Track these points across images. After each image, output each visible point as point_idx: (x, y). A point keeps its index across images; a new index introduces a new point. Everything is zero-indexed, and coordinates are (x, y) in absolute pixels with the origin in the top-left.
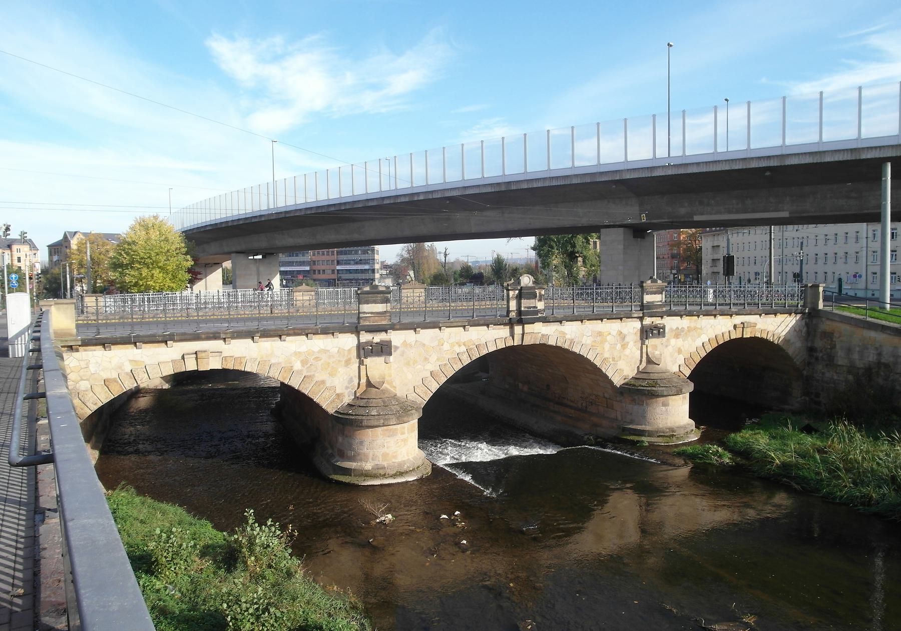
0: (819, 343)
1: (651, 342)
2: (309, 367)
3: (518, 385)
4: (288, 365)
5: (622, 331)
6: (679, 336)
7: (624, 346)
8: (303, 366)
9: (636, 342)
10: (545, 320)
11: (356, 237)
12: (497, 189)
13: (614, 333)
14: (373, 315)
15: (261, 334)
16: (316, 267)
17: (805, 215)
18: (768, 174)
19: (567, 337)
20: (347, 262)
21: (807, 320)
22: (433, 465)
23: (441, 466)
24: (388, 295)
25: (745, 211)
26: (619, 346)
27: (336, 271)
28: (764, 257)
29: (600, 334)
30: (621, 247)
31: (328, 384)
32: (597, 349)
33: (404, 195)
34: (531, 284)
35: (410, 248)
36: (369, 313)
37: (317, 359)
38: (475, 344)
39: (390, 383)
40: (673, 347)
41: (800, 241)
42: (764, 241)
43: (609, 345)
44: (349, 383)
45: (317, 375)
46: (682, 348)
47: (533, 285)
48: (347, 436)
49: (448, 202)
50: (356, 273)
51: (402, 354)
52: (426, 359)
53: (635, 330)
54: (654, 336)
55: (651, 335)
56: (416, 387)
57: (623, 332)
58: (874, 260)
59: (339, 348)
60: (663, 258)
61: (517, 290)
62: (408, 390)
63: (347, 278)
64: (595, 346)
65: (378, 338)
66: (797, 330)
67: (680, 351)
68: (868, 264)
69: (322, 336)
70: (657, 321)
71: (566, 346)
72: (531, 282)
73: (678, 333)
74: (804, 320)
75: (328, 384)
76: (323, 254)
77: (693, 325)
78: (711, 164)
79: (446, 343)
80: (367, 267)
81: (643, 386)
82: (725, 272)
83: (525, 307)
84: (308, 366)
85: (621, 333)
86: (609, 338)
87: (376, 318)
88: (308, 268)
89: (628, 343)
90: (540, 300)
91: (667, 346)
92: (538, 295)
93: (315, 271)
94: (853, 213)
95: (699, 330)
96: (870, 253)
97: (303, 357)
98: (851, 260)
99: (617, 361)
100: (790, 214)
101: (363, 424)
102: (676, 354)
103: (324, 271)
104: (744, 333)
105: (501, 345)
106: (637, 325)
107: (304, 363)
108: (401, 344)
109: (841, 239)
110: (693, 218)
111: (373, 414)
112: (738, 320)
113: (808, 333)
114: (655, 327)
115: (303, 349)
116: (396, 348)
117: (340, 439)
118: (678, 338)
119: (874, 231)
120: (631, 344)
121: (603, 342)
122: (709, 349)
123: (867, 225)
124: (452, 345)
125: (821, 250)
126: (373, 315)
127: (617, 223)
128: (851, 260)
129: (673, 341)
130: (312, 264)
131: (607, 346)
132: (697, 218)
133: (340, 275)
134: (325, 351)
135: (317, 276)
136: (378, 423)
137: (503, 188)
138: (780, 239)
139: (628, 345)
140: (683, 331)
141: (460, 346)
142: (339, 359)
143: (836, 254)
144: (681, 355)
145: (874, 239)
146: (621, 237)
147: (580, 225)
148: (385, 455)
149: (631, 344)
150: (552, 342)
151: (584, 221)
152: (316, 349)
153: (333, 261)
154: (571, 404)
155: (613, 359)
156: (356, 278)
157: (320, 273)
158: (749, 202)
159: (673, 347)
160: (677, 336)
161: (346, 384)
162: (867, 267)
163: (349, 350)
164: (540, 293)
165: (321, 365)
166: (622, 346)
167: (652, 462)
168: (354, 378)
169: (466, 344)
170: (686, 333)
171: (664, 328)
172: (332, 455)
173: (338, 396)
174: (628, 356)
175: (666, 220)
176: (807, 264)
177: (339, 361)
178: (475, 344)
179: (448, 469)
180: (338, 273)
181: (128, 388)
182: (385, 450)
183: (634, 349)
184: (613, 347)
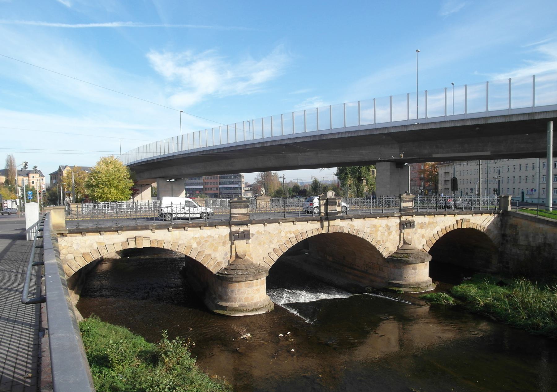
0: (508, 232)
1: (406, 231)
4: (189, 245)
5: (388, 224)
7: (390, 234)
8: (198, 245)
11: (230, 168)
12: (314, 139)
15: (173, 227)
16: (207, 186)
17: (500, 153)
18: (477, 128)
20: (225, 183)
26: (386, 234)
29: (375, 226)
30: (389, 173)
31: (213, 256)
34: (333, 196)
35: (263, 175)
36: (236, 214)
37: (206, 241)
38: (300, 233)
42: (501, 167)
47: (334, 197)
49: (284, 147)
51: (257, 238)
52: (271, 242)
54: (407, 227)
55: (406, 227)
59: (219, 235)
60: (415, 180)
62: (260, 260)
65: (242, 229)
67: (423, 236)
68: (540, 183)
71: (354, 234)
72: (334, 195)
73: (422, 226)
75: (213, 256)
77: (431, 221)
80: (237, 186)
81: (401, 258)
84: (201, 245)
88: (202, 187)
89: (392, 231)
91: (415, 233)
92: (337, 203)
93: (206, 188)
97: (198, 240)
98: (530, 181)
99: (385, 243)
100: (491, 153)
103: (211, 188)
104: (463, 225)
105: (316, 233)
106: (397, 220)
107: (198, 243)
109: (523, 167)
116: (253, 235)
117: (220, 289)
120: (394, 232)
121: (376, 231)
122: (441, 235)
124: (286, 233)
127: (386, 159)
128: (530, 181)
129: (419, 231)
130: (204, 184)
131: (379, 233)
132: (434, 156)
133: (221, 191)
134: (211, 237)
135: (207, 192)
136: (242, 279)
137: (317, 139)
141: (291, 233)
143: (514, 177)
144: (424, 239)
145: (544, 168)
146: (389, 168)
147: (364, 161)
149: (394, 232)
151: (366, 158)
155: (383, 241)
157: (209, 190)
160: (422, 227)
163: (225, 236)
164: (339, 202)
168: (228, 252)
169: (295, 232)
171: (413, 222)
173: (219, 263)
174: (392, 239)
175: (416, 157)
176: (502, 183)
180: (220, 190)
184: (383, 234)
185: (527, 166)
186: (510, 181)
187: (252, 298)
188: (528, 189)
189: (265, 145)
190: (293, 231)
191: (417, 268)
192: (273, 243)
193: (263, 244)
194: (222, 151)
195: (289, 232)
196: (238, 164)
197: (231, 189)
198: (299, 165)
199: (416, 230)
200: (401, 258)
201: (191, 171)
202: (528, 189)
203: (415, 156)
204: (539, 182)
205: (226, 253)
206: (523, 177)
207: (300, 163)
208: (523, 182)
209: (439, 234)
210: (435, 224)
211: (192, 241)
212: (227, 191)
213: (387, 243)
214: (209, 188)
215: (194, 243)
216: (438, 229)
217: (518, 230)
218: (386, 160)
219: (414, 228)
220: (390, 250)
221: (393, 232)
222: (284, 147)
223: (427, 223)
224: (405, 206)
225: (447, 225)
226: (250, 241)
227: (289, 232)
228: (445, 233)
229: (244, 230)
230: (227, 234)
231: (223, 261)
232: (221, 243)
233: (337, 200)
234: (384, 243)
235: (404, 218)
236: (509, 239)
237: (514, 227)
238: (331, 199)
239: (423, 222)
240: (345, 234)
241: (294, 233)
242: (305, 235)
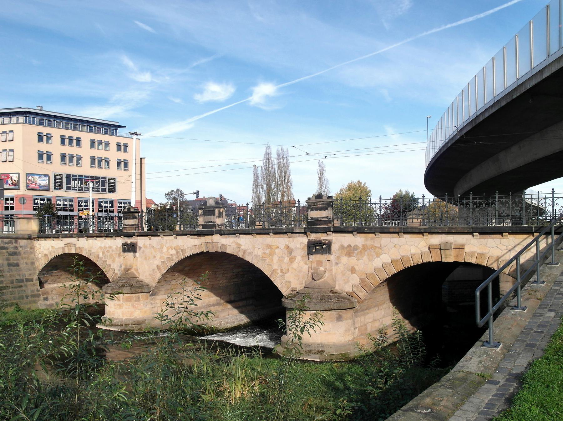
1: (316, 258)
5: (289, 245)
6: (352, 255)
7: (292, 260)
9: (303, 257)
10: (221, 233)
13: (282, 247)
26: (286, 259)
29: (269, 247)
32: (265, 260)
36: (126, 225)
39: (136, 270)
40: (344, 265)
43: (277, 258)
44: (120, 268)
53: (302, 246)
54: (317, 252)
56: (354, 286)
64: (265, 257)
70: (323, 237)
73: (350, 251)
77: (369, 243)
79: (164, 247)
83: (205, 222)
85: (289, 247)
86: (277, 251)
87: (129, 228)
95: (377, 249)
99: (285, 273)
102: (350, 273)
106: (303, 240)
107: (103, 253)
112: (436, 240)
115: (103, 245)
116: (140, 248)
120: (299, 258)
121: (272, 254)
124: (168, 249)
131: (276, 258)
134: (110, 247)
139: (295, 259)
140: (357, 249)
144: (354, 275)
149: (299, 258)
150: (229, 251)
159: (344, 265)
166: (289, 259)
169: (176, 248)
170: (361, 252)
183: (302, 263)
184: (281, 260)
216: (386, 258)
220: (293, 286)
223: (360, 246)
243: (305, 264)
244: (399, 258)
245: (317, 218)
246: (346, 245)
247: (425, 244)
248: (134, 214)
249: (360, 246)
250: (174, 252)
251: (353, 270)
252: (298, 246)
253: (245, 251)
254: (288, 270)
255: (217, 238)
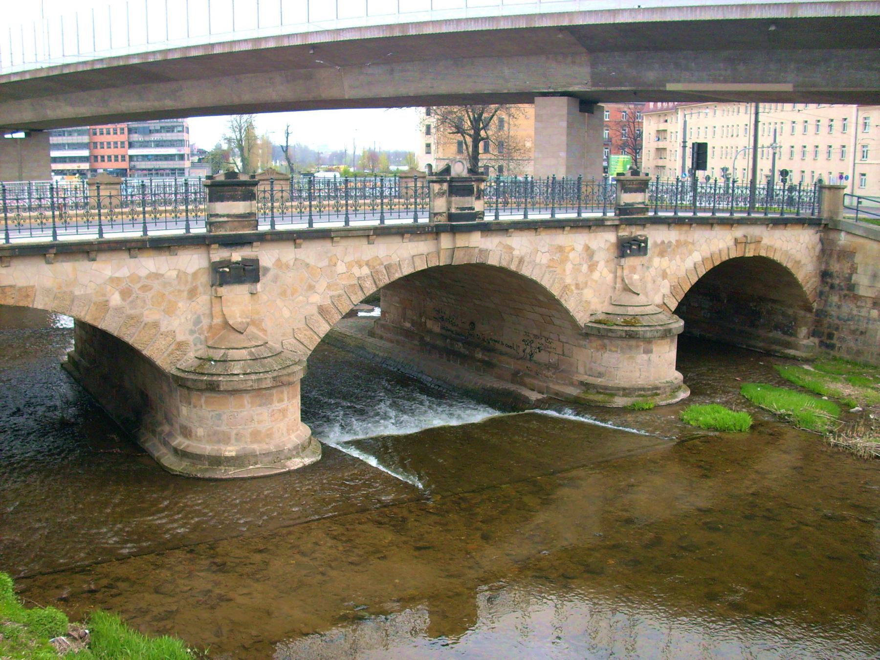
0: (835, 267)
1: (629, 262)
2: (132, 302)
3: (425, 322)
4: (101, 298)
5: (590, 245)
7: (592, 267)
8: (123, 299)
11: (169, 104)
12: (387, 34)
14: (230, 219)
15: (57, 250)
17: (812, 89)
18: (772, 28)
19: (514, 253)
20: (145, 144)
21: (822, 234)
22: (322, 444)
23: (333, 446)
24: (253, 188)
25: (735, 81)
26: (585, 268)
27: (127, 159)
28: (724, 148)
29: (561, 249)
30: (564, 124)
31: (163, 329)
33: (246, 41)
34: (465, 174)
35: (235, 124)
36: (223, 216)
37: (145, 288)
38: (382, 264)
41: (772, 127)
42: (725, 126)
45: (146, 313)
46: (668, 271)
47: (468, 176)
48: (195, 407)
49: (312, 52)
50: (156, 160)
51: (276, 279)
52: (311, 288)
54: (632, 254)
55: (628, 251)
57: (591, 247)
58: (863, 157)
59: (179, 271)
61: (445, 181)
62: (284, 335)
63: (144, 167)
65: (237, 256)
66: (810, 247)
67: (664, 275)
68: (856, 162)
69: (152, 253)
70: (637, 232)
71: (513, 267)
72: (466, 171)
73: (664, 250)
74: (819, 234)
75: (163, 329)
76: (109, 133)
77: (683, 238)
78: (698, 10)
81: (617, 325)
82: (694, 166)
84: (131, 299)
89: (598, 262)
90: (478, 198)
91: (648, 268)
92: (475, 189)
93: (96, 157)
94: (874, 90)
96: (859, 147)
97: (123, 285)
98: (836, 155)
99: (582, 289)
100: (794, 86)
101: (221, 387)
102: (660, 279)
104: (747, 251)
105: (421, 266)
106: (611, 237)
107: (125, 294)
108: (273, 265)
109: (837, 125)
110: (665, 86)
111: (236, 372)
113: (823, 251)
114: (634, 240)
116: (267, 270)
117: (184, 410)
118: (663, 256)
119: (865, 118)
120: (601, 265)
121: (564, 260)
122: (702, 272)
123: (858, 110)
124: (349, 266)
125: (798, 140)
126: (230, 219)
127: (560, 90)
128: (836, 155)
129: (656, 261)
131: (569, 266)
132: (670, 87)
133: (133, 163)
134: (157, 276)
136: (245, 385)
137: (397, 33)
138: (746, 125)
140: (670, 247)
141: (360, 266)
142: (178, 287)
143: (817, 147)
144: (666, 281)
145: (865, 129)
146: (564, 111)
147: (506, 91)
148: (256, 436)
149: (601, 265)
150: (493, 261)
151: (512, 86)
152: (143, 273)
153: (122, 143)
154: (508, 350)
155: (577, 286)
156: (157, 167)
157: (104, 161)
158: (741, 68)
159: (656, 269)
160: (662, 254)
161: (190, 326)
162: (854, 166)
163: (195, 274)
164: (478, 187)
165: (152, 298)
167: (633, 433)
168: (202, 317)
169: (370, 263)
171: (645, 241)
172: (170, 434)
173: (180, 345)
174: (596, 282)
176: (780, 159)
177: (179, 291)
178: (382, 264)
179: (355, 453)
181: (775, 259)
182: (255, 425)
183: (605, 272)
184: (577, 269)
185: (831, 126)
186: (807, 155)
187: (268, 432)
188: (830, 173)
189: (263, 46)
190: (366, 259)
191: (654, 350)
192: (319, 291)
193: (293, 294)
194: (152, 60)
195: (356, 262)
196: (191, 96)
197: (157, 158)
198: (347, 97)
199: (650, 260)
200: (617, 325)
201: (66, 110)
202: (830, 173)
203: (625, 86)
204: (854, 160)
205: (199, 317)
206: (836, 146)
207: (349, 94)
208: (809, 157)
209: (698, 270)
210: (690, 246)
211: (109, 288)
212: (149, 163)
213: (585, 291)
214: (103, 157)
215: (113, 294)
216: (697, 257)
217: (857, 264)
218: (559, 92)
219: (645, 254)
220: (593, 307)
221: (599, 265)
222: (312, 52)
223: (674, 242)
224: (627, 202)
225: (714, 248)
226: (259, 286)
227: (356, 262)
228: (710, 267)
229: (242, 259)
230: (200, 269)
231: (191, 339)
232: (183, 291)
233: (473, 183)
234: (578, 292)
235: (625, 232)
236: (837, 282)
237: (847, 254)
238: (460, 179)
239: (666, 242)
240: (493, 267)
241: (367, 264)
242: (396, 271)
243: (610, 272)
244: (709, 256)
245: (632, 204)
246: (659, 242)
247: (730, 238)
248: (250, 188)
249: (674, 242)
250: (365, 271)
251: (664, 275)
252: (602, 245)
253: (521, 261)
254: (586, 283)
255: (476, 240)
